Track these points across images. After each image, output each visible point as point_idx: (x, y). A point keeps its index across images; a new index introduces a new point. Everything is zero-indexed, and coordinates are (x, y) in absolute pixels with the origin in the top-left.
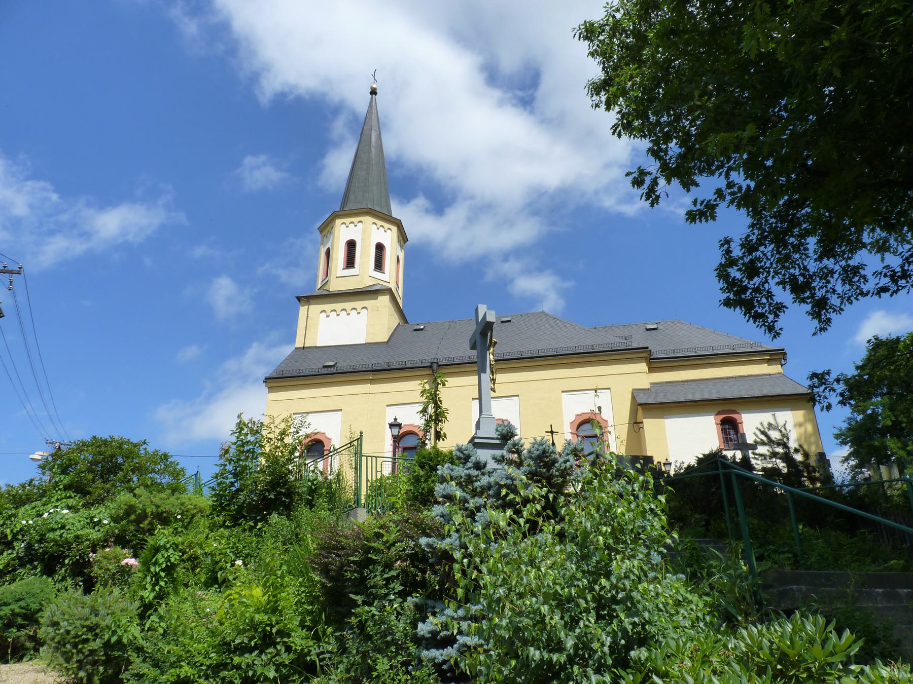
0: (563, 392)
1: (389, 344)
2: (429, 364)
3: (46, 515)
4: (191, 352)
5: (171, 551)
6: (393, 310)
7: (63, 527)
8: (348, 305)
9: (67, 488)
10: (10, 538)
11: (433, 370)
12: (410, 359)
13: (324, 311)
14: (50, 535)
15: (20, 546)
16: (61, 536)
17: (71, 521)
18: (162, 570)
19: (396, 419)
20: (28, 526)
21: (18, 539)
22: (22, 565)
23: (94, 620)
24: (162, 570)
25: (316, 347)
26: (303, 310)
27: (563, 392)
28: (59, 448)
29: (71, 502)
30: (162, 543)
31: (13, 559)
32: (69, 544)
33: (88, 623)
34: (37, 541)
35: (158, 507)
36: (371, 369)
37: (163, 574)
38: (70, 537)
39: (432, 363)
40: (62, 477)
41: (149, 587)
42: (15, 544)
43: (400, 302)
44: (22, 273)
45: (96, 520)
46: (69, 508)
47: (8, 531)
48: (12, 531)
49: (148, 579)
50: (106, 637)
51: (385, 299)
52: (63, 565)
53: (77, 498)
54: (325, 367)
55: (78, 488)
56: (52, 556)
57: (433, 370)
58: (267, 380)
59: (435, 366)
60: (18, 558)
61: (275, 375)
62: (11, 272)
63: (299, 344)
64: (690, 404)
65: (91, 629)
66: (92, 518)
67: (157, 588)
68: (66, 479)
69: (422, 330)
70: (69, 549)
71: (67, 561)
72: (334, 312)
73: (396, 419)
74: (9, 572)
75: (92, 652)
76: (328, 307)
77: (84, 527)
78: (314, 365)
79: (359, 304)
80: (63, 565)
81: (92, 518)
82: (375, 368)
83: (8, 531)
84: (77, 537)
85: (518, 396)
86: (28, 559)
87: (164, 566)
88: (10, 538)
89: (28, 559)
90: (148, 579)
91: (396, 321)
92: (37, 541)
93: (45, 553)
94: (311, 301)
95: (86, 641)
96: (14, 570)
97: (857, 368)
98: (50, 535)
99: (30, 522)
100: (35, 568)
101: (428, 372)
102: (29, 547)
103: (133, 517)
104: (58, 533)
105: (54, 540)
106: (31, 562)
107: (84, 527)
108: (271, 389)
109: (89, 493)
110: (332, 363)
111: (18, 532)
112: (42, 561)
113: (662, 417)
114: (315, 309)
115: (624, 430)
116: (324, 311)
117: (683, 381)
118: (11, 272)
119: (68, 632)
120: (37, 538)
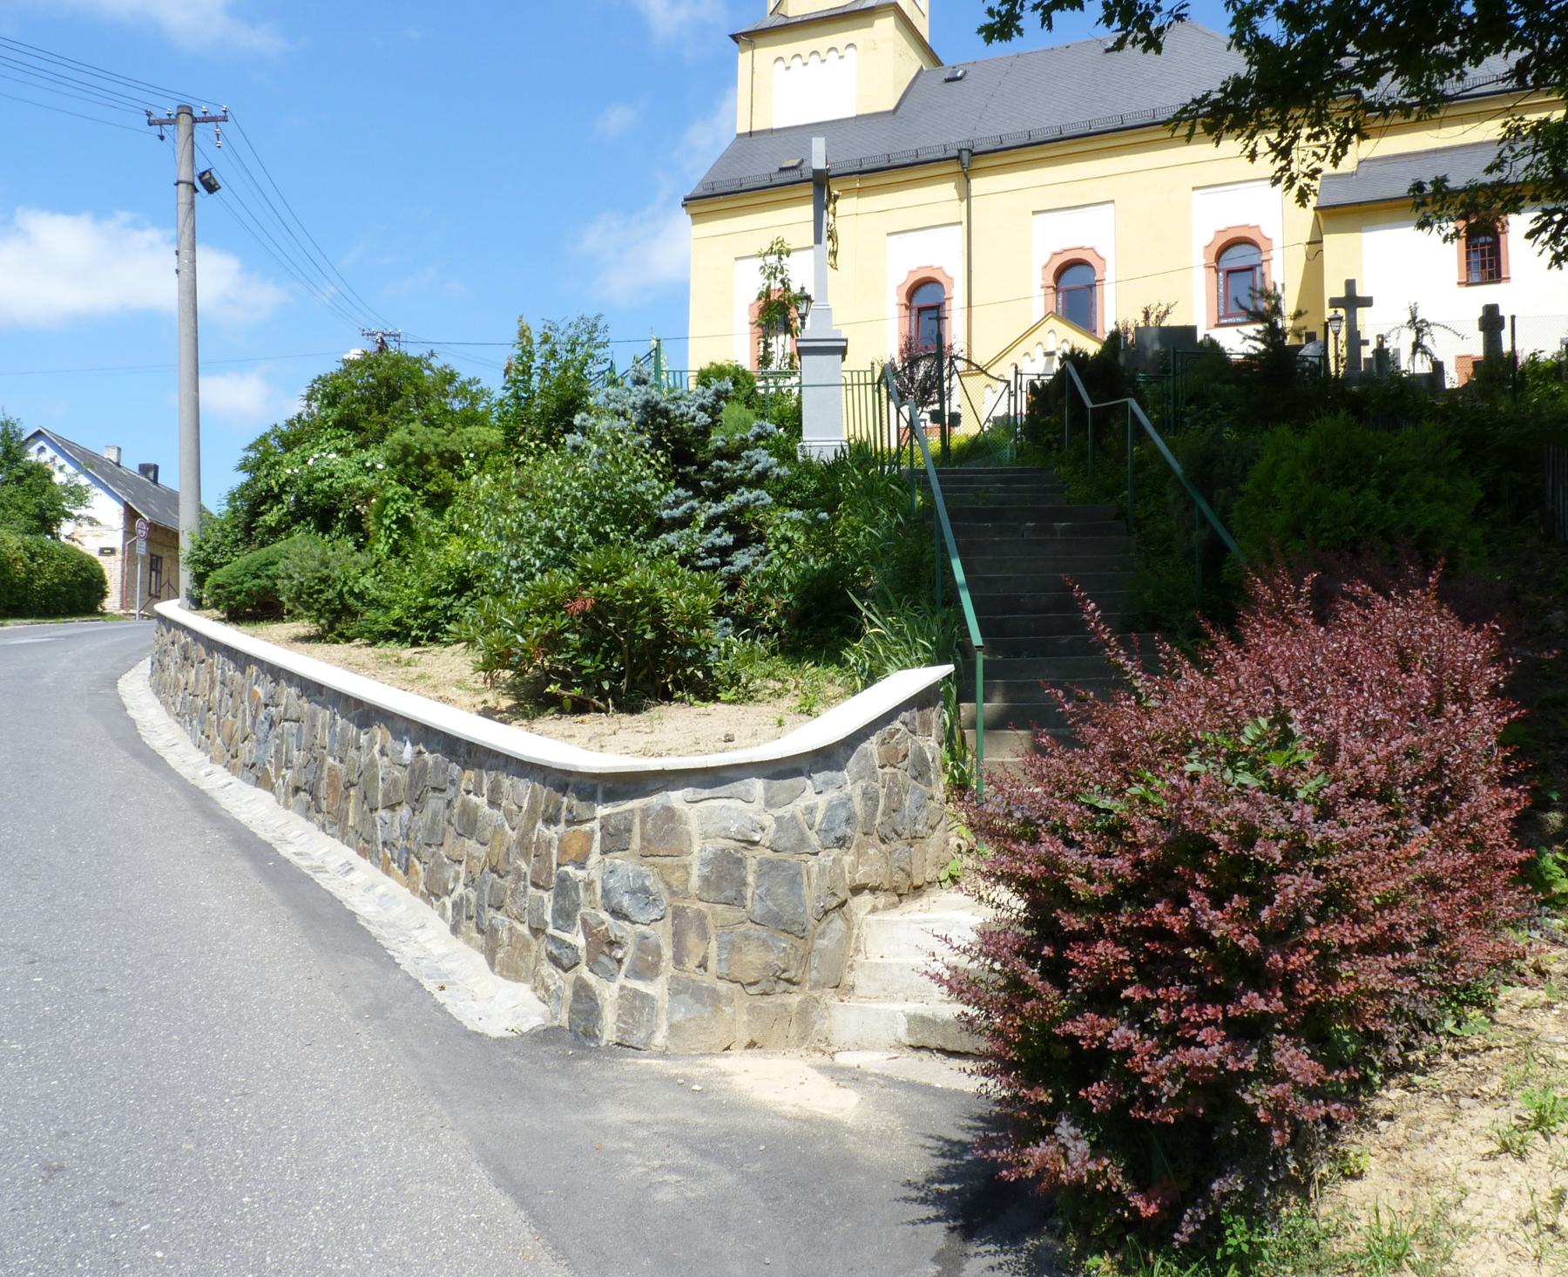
0: (1194, 189)
1: (897, 114)
2: (955, 153)
3: (310, 462)
4: (618, 119)
5: (401, 502)
6: (905, 43)
7: (331, 475)
8: (822, 42)
9: (337, 424)
10: (276, 490)
11: (962, 164)
12: (923, 145)
13: (780, 59)
14: (318, 485)
15: (290, 499)
16: (330, 486)
17: (340, 467)
18: (394, 522)
19: (803, 289)
20: (294, 475)
21: (286, 492)
22: (296, 522)
23: (325, 572)
24: (394, 522)
25: (772, 131)
26: (744, 58)
27: (1194, 189)
28: (383, 341)
29: (341, 444)
30: (389, 494)
31: (285, 515)
32: (340, 495)
33: (318, 575)
34: (305, 493)
35: (436, 445)
36: (857, 168)
37: (394, 527)
38: (338, 486)
39: (960, 151)
40: (330, 411)
41: (383, 539)
42: (284, 497)
43: (923, 27)
44: (230, 118)
45: (368, 464)
46: (338, 451)
47: (273, 483)
48: (277, 482)
49: (382, 532)
50: (339, 587)
51: (886, 25)
52: (339, 520)
53: (350, 437)
54: (782, 170)
55: (348, 423)
56: (322, 509)
57: (962, 164)
58: (689, 201)
59: (965, 155)
60: (289, 513)
61: (701, 192)
62: (214, 119)
63: (743, 128)
64: (1398, 203)
65: (323, 580)
66: (364, 462)
67: (391, 541)
68: (334, 413)
69: (960, 79)
70: (341, 501)
71: (341, 515)
72: (797, 59)
73: (803, 289)
74: (284, 530)
75: (328, 601)
76: (786, 49)
77: (355, 475)
78: (763, 168)
79: (840, 39)
80: (339, 520)
81: (364, 462)
82: (865, 167)
83: (273, 483)
84: (347, 486)
85: (1113, 201)
86: (300, 514)
87: (394, 518)
88: (276, 490)
89: (300, 514)
90: (382, 532)
91: (913, 62)
92: (305, 493)
93: (315, 506)
94: (757, 41)
95: (321, 592)
96: (289, 527)
97: (243, 467)
98: (318, 485)
99: (296, 471)
100: (309, 524)
101: (955, 168)
102: (298, 500)
103: (410, 459)
104: (326, 482)
105: (323, 491)
106: (303, 517)
107: (355, 475)
108: (697, 217)
109: (363, 429)
110: (794, 162)
111: (284, 483)
112: (314, 516)
113: (1358, 229)
114: (765, 54)
115: (1300, 255)
116: (780, 59)
117: (1428, 152)
118: (214, 119)
119: (302, 583)
120: (305, 489)
